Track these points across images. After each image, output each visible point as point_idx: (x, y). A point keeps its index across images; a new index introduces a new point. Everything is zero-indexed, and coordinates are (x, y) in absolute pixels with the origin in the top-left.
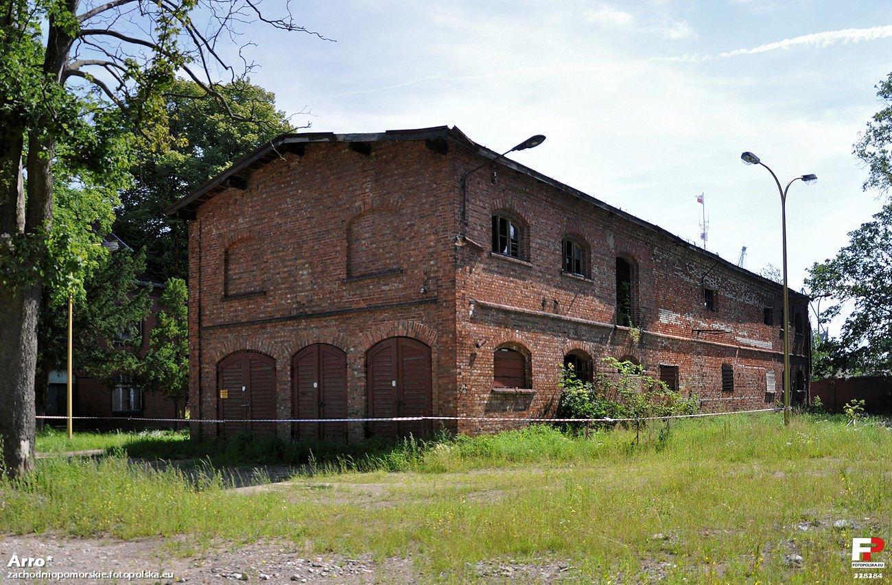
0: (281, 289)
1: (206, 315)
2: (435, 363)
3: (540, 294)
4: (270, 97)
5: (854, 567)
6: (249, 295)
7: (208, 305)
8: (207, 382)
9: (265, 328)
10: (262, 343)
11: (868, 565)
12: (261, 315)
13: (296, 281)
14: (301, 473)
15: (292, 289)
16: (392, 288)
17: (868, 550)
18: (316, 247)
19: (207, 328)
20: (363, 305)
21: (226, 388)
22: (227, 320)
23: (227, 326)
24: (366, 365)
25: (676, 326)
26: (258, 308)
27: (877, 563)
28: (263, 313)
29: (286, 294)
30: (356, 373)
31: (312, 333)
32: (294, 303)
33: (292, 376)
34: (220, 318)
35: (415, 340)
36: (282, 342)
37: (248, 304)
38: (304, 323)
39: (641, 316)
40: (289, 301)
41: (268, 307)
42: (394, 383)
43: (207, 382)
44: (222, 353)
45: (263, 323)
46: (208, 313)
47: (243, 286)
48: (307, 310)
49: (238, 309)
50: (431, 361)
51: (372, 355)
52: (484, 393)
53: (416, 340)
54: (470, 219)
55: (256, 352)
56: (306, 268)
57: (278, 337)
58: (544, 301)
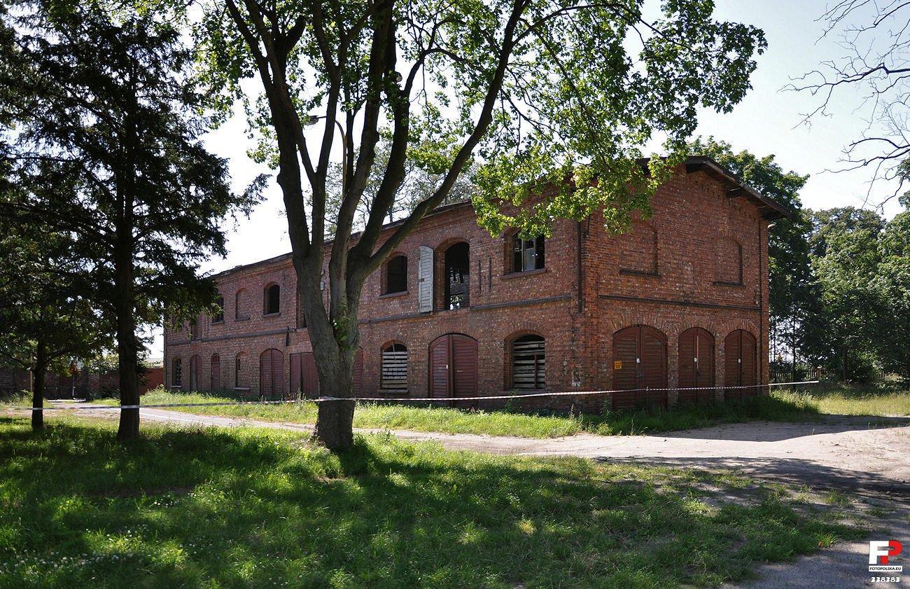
0: (672, 277)
1: (602, 283)
5: (872, 571)
7: (604, 274)
8: (604, 353)
9: (659, 308)
11: (885, 569)
12: (655, 296)
14: (829, 397)
15: (680, 279)
17: (885, 553)
18: (696, 251)
21: (620, 359)
22: (624, 293)
23: (623, 298)
26: (654, 288)
27: (895, 567)
28: (657, 294)
29: (676, 282)
32: (681, 291)
34: (617, 290)
37: (645, 283)
38: (688, 309)
40: (678, 289)
41: (661, 290)
43: (604, 353)
44: (619, 324)
46: (604, 281)
47: (634, 263)
48: (690, 299)
53: (750, 333)
56: (689, 265)
57: (669, 318)
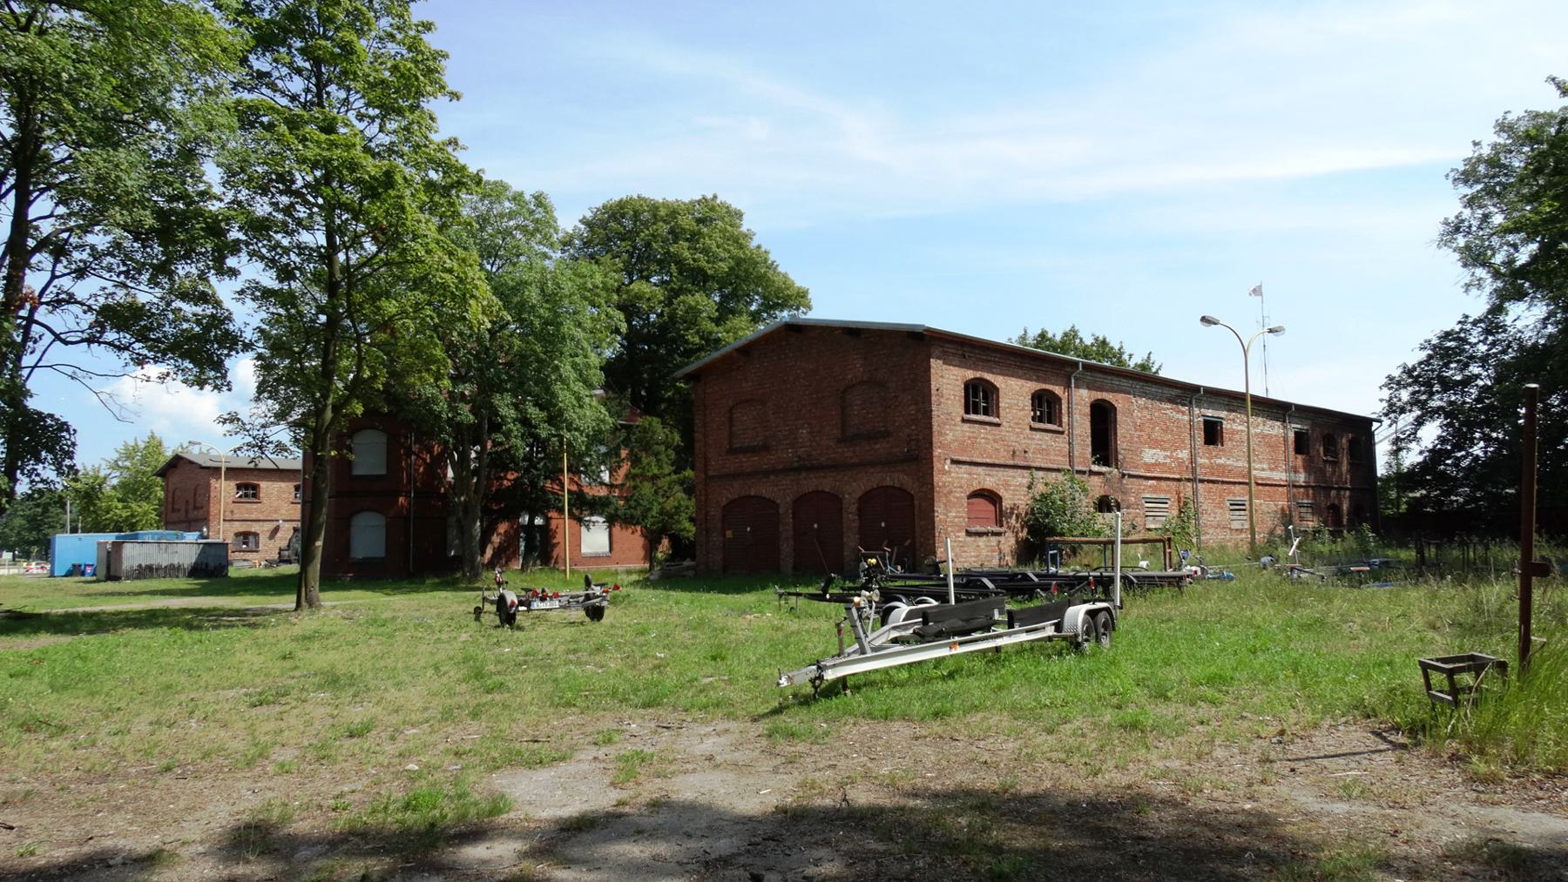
2: (917, 508)
3: (1009, 446)
4: (739, 215)
6: (752, 450)
10: (766, 489)
13: (796, 438)
16: (881, 448)
19: (713, 477)
20: (856, 460)
23: (1343, 755)
24: (859, 509)
25: (1165, 464)
30: (851, 517)
31: (811, 483)
33: (793, 518)
35: (900, 489)
36: (785, 490)
39: (1120, 457)
42: (883, 525)
44: (727, 498)
45: (766, 473)
47: (747, 441)
49: (748, 462)
50: (914, 507)
51: (866, 499)
52: (959, 531)
54: (945, 391)
55: (761, 498)
58: (1014, 452)
